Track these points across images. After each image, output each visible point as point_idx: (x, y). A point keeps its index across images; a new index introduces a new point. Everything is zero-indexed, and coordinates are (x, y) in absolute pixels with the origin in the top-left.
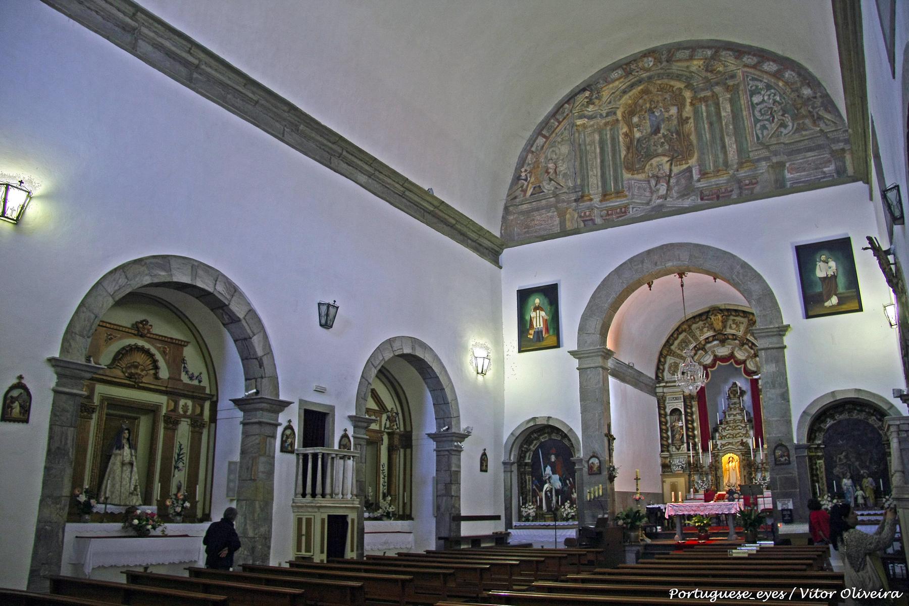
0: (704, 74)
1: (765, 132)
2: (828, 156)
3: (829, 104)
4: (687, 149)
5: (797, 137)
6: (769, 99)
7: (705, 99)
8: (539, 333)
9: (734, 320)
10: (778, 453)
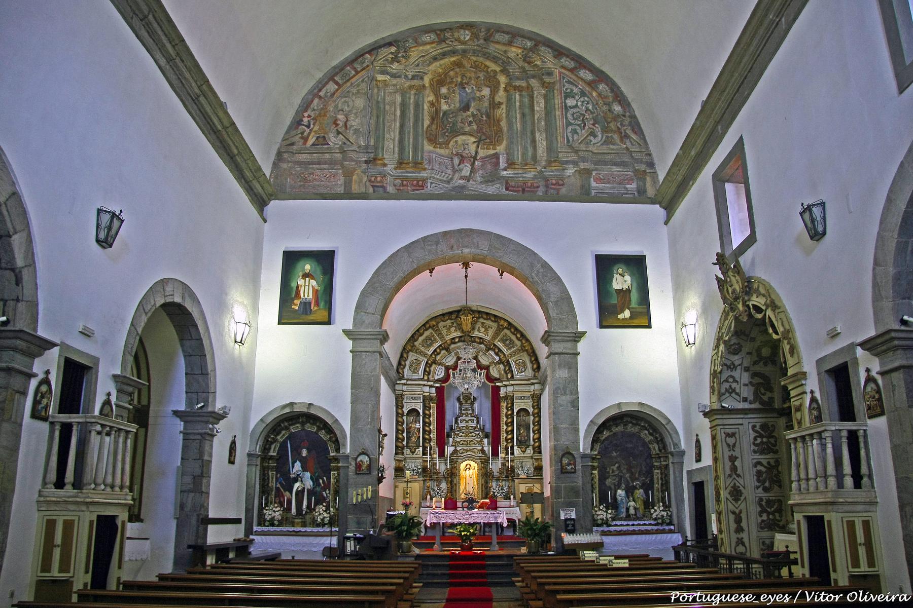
0: (521, 63)
1: (576, 137)
4: (496, 134)
5: (604, 149)
6: (582, 105)
7: (519, 89)
8: (306, 305)
9: (483, 323)
10: (565, 461)
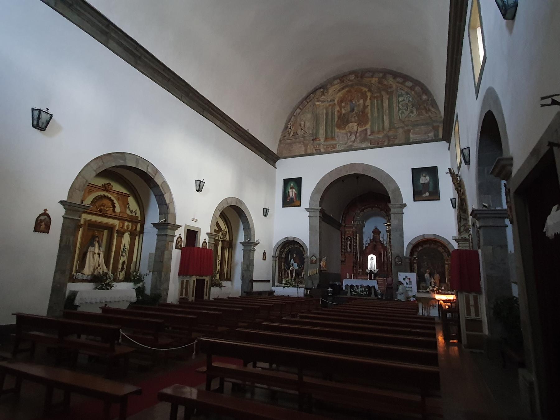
2: (431, 128)
3: (434, 104)
